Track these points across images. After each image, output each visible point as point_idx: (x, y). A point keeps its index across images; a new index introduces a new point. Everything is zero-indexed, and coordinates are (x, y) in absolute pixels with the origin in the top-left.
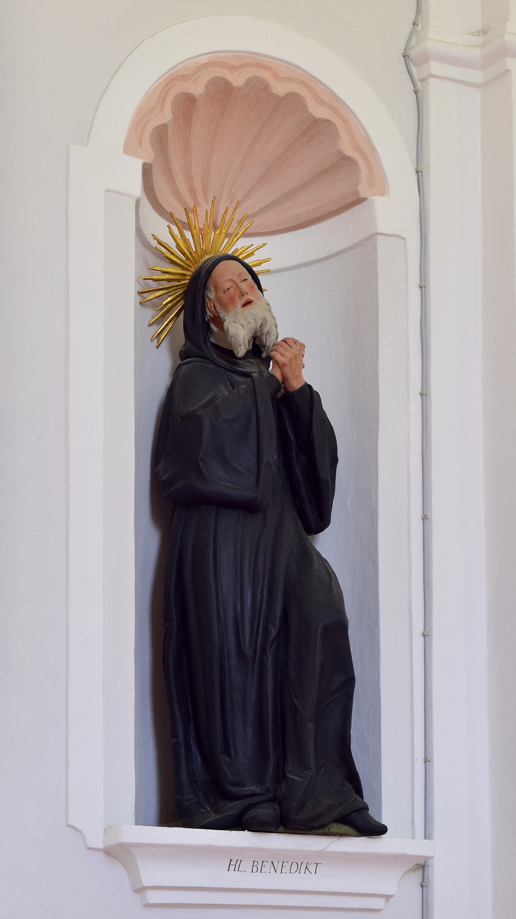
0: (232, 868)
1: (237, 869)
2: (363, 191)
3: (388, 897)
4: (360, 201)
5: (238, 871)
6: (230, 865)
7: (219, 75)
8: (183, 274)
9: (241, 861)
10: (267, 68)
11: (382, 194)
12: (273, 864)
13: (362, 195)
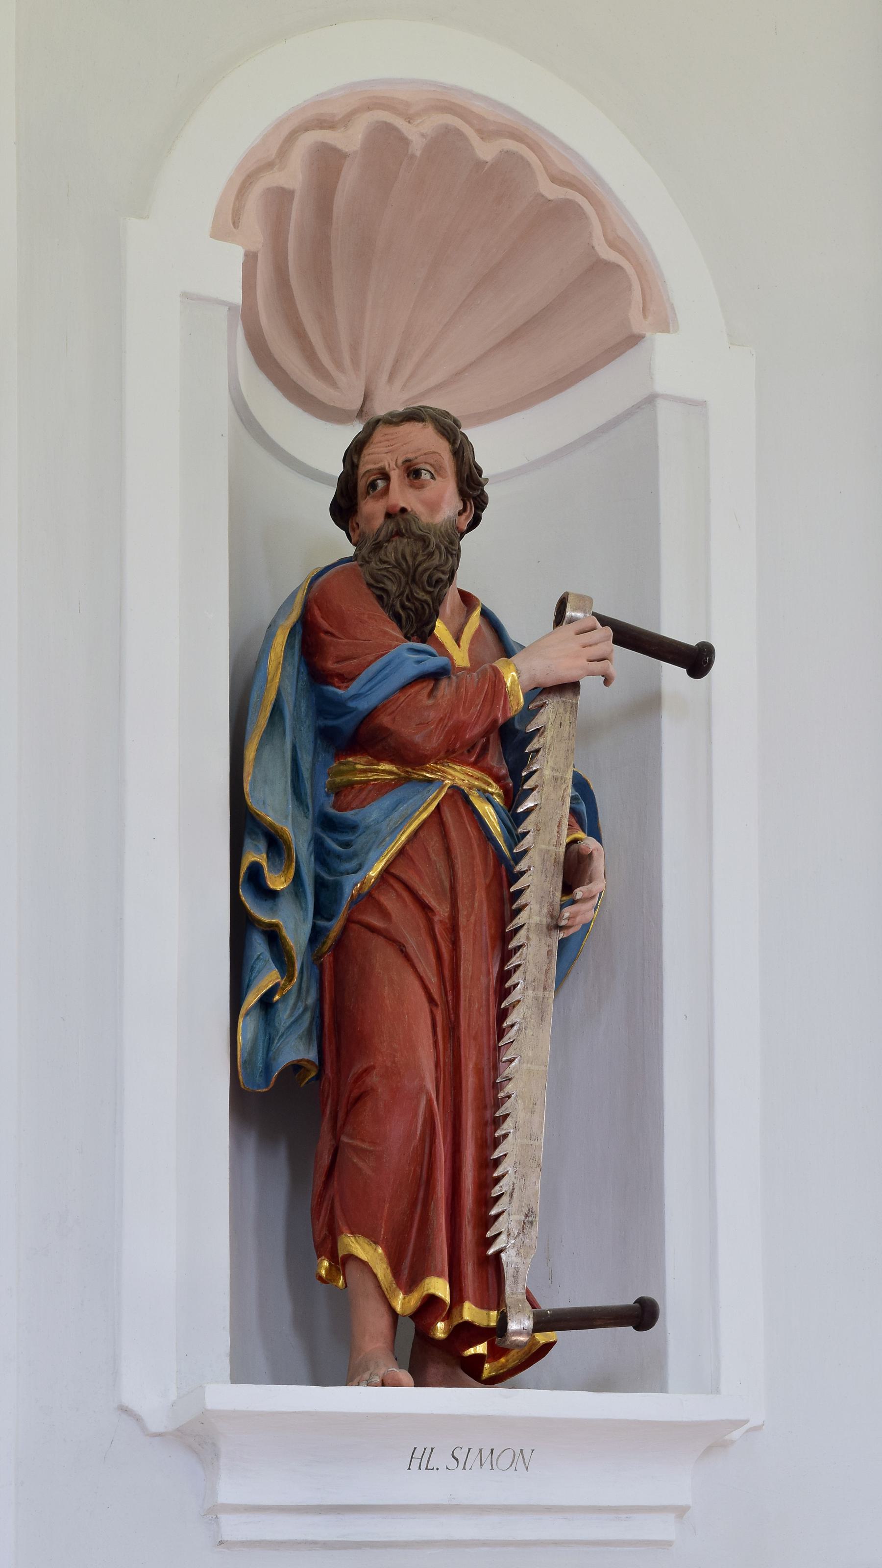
0: (415, 1462)
1: (423, 1467)
2: (637, 323)
3: (681, 1511)
4: (634, 340)
5: (426, 1469)
6: (412, 1458)
7: (384, 119)
8: (260, 426)
9: (432, 1449)
10: (534, 147)
11: (666, 330)
12: (522, 1454)
13: (636, 329)
